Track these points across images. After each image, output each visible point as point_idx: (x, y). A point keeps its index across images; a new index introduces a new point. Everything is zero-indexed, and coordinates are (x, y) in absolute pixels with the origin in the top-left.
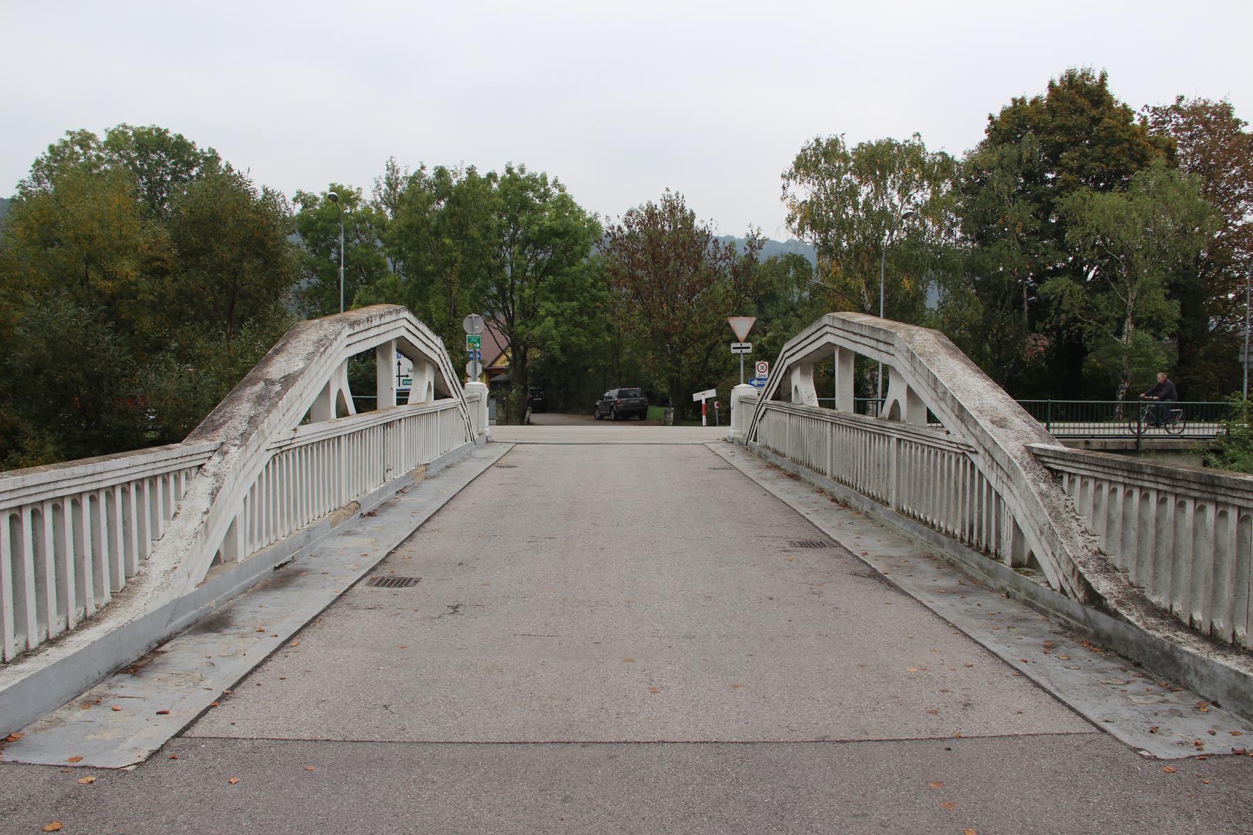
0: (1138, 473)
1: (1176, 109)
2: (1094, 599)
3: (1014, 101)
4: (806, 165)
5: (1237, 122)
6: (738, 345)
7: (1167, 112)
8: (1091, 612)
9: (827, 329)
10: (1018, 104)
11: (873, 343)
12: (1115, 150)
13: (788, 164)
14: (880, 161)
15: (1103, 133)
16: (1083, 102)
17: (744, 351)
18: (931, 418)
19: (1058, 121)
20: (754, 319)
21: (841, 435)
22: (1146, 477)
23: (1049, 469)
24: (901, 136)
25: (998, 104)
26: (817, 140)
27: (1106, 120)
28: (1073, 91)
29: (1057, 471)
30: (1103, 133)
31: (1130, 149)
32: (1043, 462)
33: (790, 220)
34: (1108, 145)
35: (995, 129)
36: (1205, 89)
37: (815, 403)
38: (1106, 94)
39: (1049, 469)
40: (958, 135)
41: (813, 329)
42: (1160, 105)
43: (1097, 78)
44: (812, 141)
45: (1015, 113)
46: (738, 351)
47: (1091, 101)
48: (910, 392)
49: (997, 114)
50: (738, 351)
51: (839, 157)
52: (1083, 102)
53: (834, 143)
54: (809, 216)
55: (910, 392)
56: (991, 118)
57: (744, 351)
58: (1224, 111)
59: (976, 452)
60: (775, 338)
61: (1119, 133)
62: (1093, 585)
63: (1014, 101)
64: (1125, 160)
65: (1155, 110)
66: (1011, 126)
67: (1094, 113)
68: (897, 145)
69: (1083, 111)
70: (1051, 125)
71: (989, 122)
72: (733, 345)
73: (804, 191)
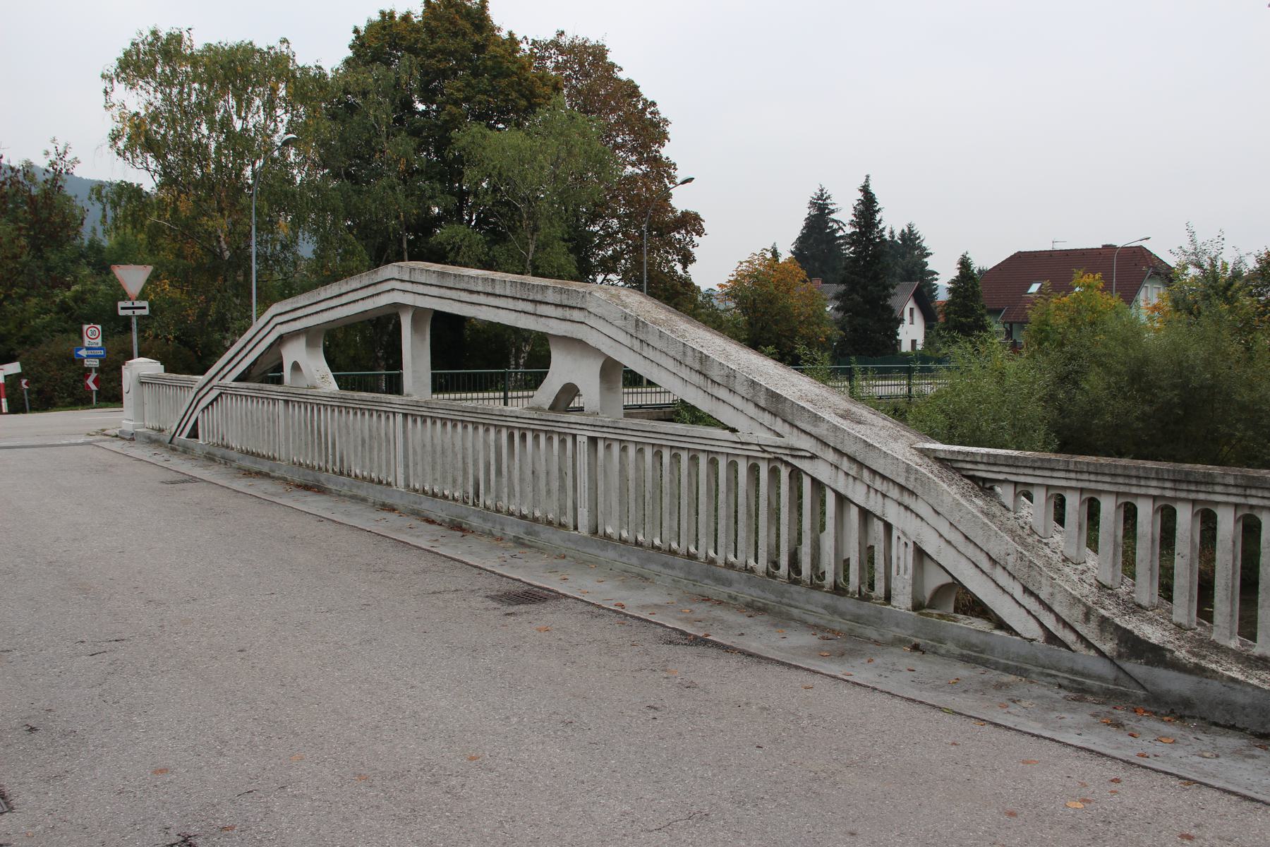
0: (1207, 483)
1: (555, 44)
2: (1135, 647)
3: (383, 13)
4: (133, 66)
5: (613, 65)
6: (129, 304)
7: (546, 47)
8: (1137, 668)
10: (387, 17)
11: (529, 307)
12: (504, 82)
13: (111, 63)
14: (237, 70)
15: (489, 63)
17: (138, 312)
19: (439, 43)
20: (150, 268)
21: (421, 433)
22: (1218, 489)
23: (973, 478)
25: (365, 13)
26: (154, 33)
27: (491, 48)
28: (452, 10)
29: (985, 480)
30: (489, 63)
31: (520, 84)
32: (958, 470)
33: (115, 137)
34: (495, 77)
35: (362, 45)
36: (583, 28)
37: (333, 386)
38: (487, 18)
39: (973, 478)
40: (325, 50)
41: (366, 281)
42: (540, 38)
44: (147, 33)
45: (384, 28)
46: (129, 312)
47: (473, 24)
49: (362, 27)
50: (129, 312)
51: (186, 58)
53: (176, 39)
54: (138, 137)
56: (356, 31)
57: (138, 312)
58: (599, 53)
59: (813, 457)
60: (83, 292)
61: (505, 65)
62: (1136, 632)
63: (383, 13)
64: (514, 95)
65: (534, 43)
67: (477, 38)
68: (259, 51)
69: (464, 34)
70: (432, 47)
71: (353, 36)
72: (121, 304)
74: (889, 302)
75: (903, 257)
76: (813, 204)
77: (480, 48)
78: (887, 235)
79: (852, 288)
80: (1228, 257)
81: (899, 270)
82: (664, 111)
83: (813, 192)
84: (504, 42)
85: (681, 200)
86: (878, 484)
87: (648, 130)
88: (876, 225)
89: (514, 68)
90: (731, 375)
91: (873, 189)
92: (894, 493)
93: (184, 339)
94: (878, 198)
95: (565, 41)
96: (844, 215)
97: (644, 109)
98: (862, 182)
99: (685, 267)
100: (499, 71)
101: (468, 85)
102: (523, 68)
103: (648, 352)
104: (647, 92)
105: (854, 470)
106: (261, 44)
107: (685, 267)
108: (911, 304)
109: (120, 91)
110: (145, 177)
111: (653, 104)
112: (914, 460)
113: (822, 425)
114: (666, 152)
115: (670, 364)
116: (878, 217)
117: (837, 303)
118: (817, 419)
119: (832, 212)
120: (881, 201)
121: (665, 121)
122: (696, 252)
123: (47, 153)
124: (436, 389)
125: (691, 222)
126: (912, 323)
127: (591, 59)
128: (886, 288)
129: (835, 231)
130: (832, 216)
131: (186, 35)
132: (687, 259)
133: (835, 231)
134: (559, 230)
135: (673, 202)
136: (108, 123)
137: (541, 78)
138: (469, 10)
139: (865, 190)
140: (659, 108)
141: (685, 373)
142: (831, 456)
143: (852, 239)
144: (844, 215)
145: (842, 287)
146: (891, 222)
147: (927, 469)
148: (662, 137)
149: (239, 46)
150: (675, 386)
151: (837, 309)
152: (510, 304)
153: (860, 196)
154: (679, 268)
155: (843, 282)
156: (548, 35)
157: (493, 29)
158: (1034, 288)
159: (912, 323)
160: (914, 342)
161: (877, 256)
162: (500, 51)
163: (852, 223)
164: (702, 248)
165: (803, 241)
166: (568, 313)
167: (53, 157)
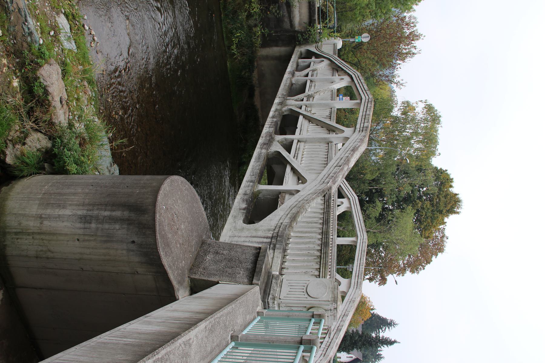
3: (452, 179)
4: (430, 109)
5: (437, 255)
7: (443, 233)
9: (367, 97)
10: (451, 180)
11: (357, 275)
12: (429, 220)
14: (430, 140)
16: (449, 207)
18: (322, 343)
24: (440, 148)
35: (441, 173)
36: (448, 245)
43: (458, 211)
44: (440, 114)
45: (447, 180)
47: (449, 210)
48: (347, 139)
52: (449, 207)
54: (408, 107)
55: (347, 139)
56: (446, 171)
58: (441, 250)
63: (452, 179)
64: (425, 224)
65: (444, 229)
66: (443, 179)
67: (444, 211)
69: (445, 207)
70: (441, 197)
71: (444, 169)
73: (420, 111)
74: (355, 349)
75: (372, 355)
76: (392, 321)
77: (441, 212)
78: (379, 349)
79: (360, 336)
81: (367, 353)
82: (422, 272)
83: (396, 321)
84: (443, 220)
85: (390, 278)
86: (325, 350)
87: (415, 266)
88: (382, 345)
89: (434, 224)
90: (344, 321)
91: (395, 344)
92: (324, 353)
94: (392, 346)
95: (445, 239)
96: (386, 333)
97: (422, 266)
98: (398, 340)
99: (368, 279)
100: (433, 219)
102: (435, 227)
103: (348, 303)
104: (428, 267)
105: (328, 345)
106: (438, 147)
107: (368, 279)
108: (354, 357)
109: (421, 106)
110: (396, 112)
111: (424, 269)
112: (330, 356)
114: (408, 273)
115: (346, 308)
116: (385, 346)
117: (355, 330)
118: (337, 338)
119: (389, 328)
120: (391, 347)
121: (418, 273)
122: (373, 283)
123: (402, 80)
124: (338, 245)
125: (383, 281)
126: (347, 357)
127: (439, 248)
128: (360, 348)
129: (382, 329)
130: (387, 328)
131: (440, 125)
132: (371, 280)
133: (382, 329)
134: (380, 240)
135: (390, 275)
136: (412, 101)
137: (431, 232)
138: (454, 208)
140: (422, 271)
141: (344, 311)
142: (330, 341)
143: (377, 337)
144: (386, 333)
145: (360, 333)
146: (384, 350)
147: (328, 359)
148: (412, 272)
150: (341, 307)
151: (353, 331)
152: (358, 270)
153: (393, 340)
154: (368, 277)
155: (362, 333)
156: (447, 233)
157: (447, 216)
159: (347, 357)
160: (340, 358)
161: (371, 345)
162: (440, 219)
163: (383, 337)
164: (374, 285)
165: (378, 317)
166: (356, 284)
167: (401, 82)
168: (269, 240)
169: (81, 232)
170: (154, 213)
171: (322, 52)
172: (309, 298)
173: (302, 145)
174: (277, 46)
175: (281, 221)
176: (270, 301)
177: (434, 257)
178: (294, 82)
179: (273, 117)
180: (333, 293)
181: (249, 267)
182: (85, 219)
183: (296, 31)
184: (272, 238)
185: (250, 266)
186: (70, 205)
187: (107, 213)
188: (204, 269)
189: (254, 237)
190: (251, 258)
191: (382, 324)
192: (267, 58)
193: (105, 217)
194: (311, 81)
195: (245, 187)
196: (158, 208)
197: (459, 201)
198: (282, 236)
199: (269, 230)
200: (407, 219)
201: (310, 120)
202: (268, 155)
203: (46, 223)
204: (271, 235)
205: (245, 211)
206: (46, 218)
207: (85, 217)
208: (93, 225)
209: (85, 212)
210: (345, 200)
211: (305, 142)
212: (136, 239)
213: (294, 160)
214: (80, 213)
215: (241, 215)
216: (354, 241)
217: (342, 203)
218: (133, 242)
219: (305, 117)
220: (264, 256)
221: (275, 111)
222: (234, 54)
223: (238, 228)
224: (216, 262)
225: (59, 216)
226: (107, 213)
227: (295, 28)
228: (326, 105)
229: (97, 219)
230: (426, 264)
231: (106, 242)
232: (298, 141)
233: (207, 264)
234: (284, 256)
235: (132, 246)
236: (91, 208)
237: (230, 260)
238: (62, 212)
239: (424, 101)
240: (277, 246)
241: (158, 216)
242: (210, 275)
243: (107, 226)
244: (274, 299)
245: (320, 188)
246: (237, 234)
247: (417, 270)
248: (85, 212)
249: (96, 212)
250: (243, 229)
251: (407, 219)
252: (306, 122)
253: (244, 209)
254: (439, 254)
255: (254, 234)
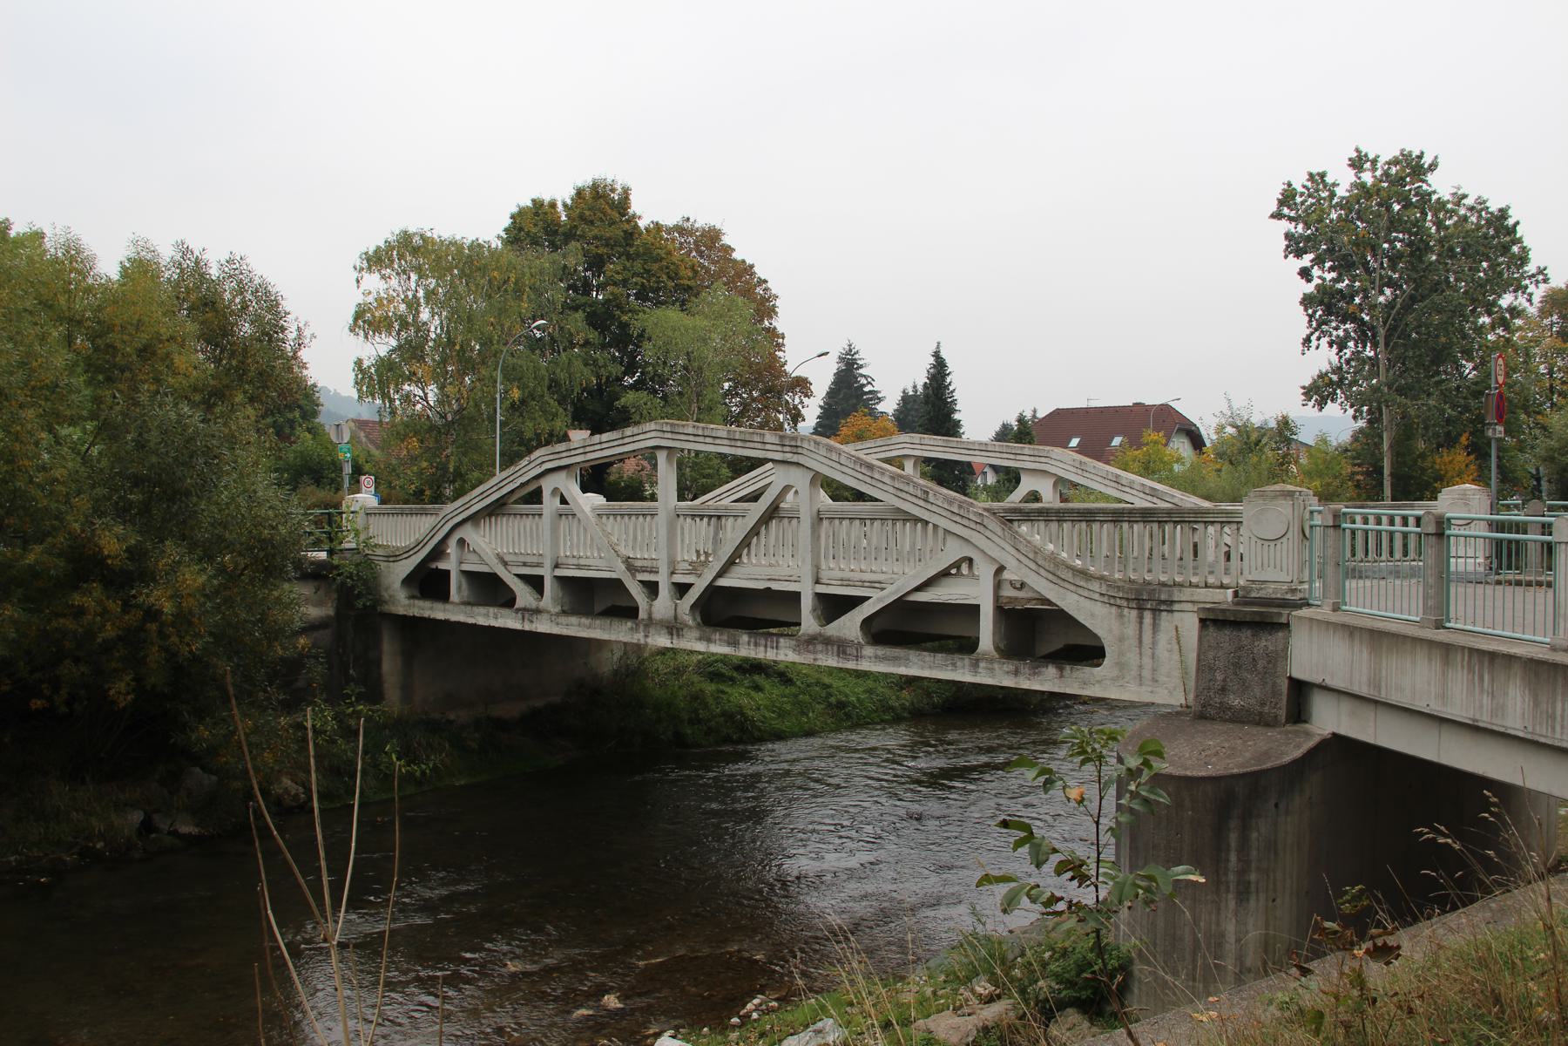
4: (376, 260)
5: (634, 216)
10: (538, 204)
12: (655, 267)
45: (537, 214)
63: (534, 201)
64: (665, 278)
66: (534, 226)
80: (1256, 420)
87: (765, 307)
88: (947, 387)
91: (943, 354)
93: (1009, 481)
94: (948, 362)
98: (933, 348)
101: (625, 268)
104: (760, 272)
111: (765, 281)
113: (1543, 453)
119: (861, 367)
120: (951, 366)
127: (711, 237)
139: (937, 355)
149: (453, 243)
153: (932, 360)
158: (1117, 441)
168: (1148, 616)
169: (1262, 897)
170: (1233, 776)
171: (420, 544)
172: (1290, 535)
173: (824, 576)
174: (379, 663)
175: (1096, 596)
176: (1298, 596)
177: (735, 255)
178: (558, 609)
179: (734, 643)
180: (1275, 497)
181: (1249, 633)
182: (1243, 894)
183: (338, 613)
184: (1141, 609)
185: (1246, 634)
186: (1218, 924)
187: (1233, 857)
188: (1263, 704)
189: (1140, 641)
190: (1226, 637)
191: (850, 386)
192: (406, 689)
193: (1239, 860)
194: (557, 566)
195: (993, 677)
196: (1221, 773)
197: (595, 186)
198: (1139, 592)
199: (1121, 616)
200: (663, 323)
201: (731, 563)
202: (868, 643)
203: (1248, 962)
204: (1134, 613)
205: (1068, 667)
206: (1242, 963)
207: (1239, 893)
208: (1253, 877)
209: (1231, 896)
210: (547, 485)
211: (817, 568)
212: (1273, 802)
213: (890, 589)
214: (1232, 904)
215: (1076, 674)
216: (669, 458)
217: (555, 491)
218: (1276, 805)
219: (720, 574)
220: (1223, 611)
221: (709, 640)
222: (435, 769)
223: (1115, 672)
224: (1245, 687)
225: (1238, 941)
226: (1233, 857)
227: (329, 617)
228: (555, 530)
229: (1243, 871)
230: (753, 274)
231: (1276, 853)
232: (817, 582)
233: (1253, 701)
234: (1181, 585)
235: (1282, 807)
236: (1223, 888)
237: (1237, 666)
238: (1231, 938)
239: (356, 275)
240: (1163, 597)
241: (1235, 771)
242: (1275, 693)
243: (1254, 853)
244: (1294, 591)
245: (999, 530)
246: (1134, 673)
247: (768, 300)
248: (1231, 896)
249: (1232, 877)
250: (1121, 665)
251: (663, 323)
252: (736, 570)
253: (1061, 670)
254: (726, 240)
255: (1135, 642)
